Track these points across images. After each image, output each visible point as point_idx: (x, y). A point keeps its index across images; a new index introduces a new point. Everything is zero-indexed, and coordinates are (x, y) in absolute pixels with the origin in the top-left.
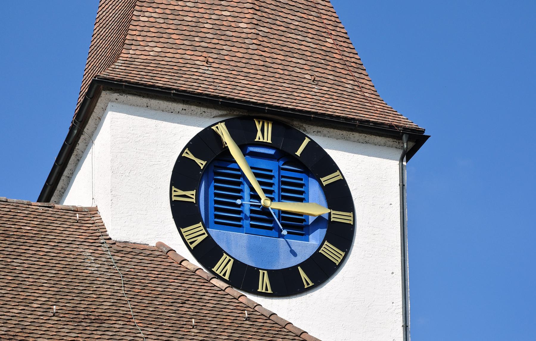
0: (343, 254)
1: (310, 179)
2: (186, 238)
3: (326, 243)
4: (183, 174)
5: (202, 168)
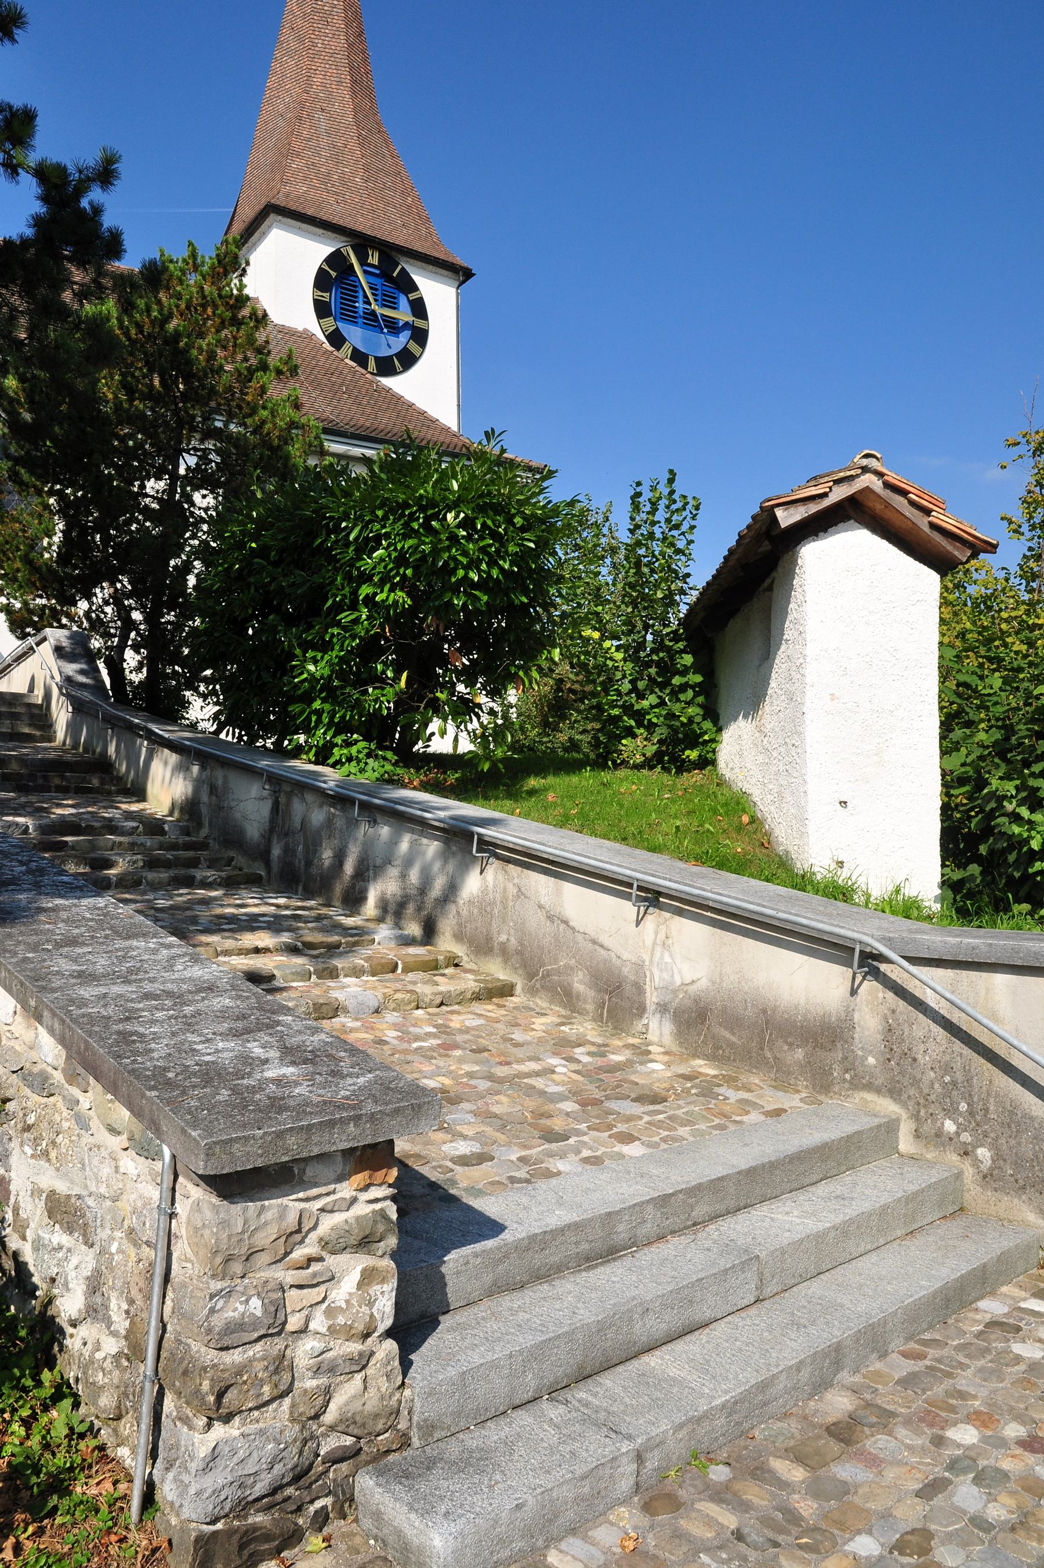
4: (322, 281)
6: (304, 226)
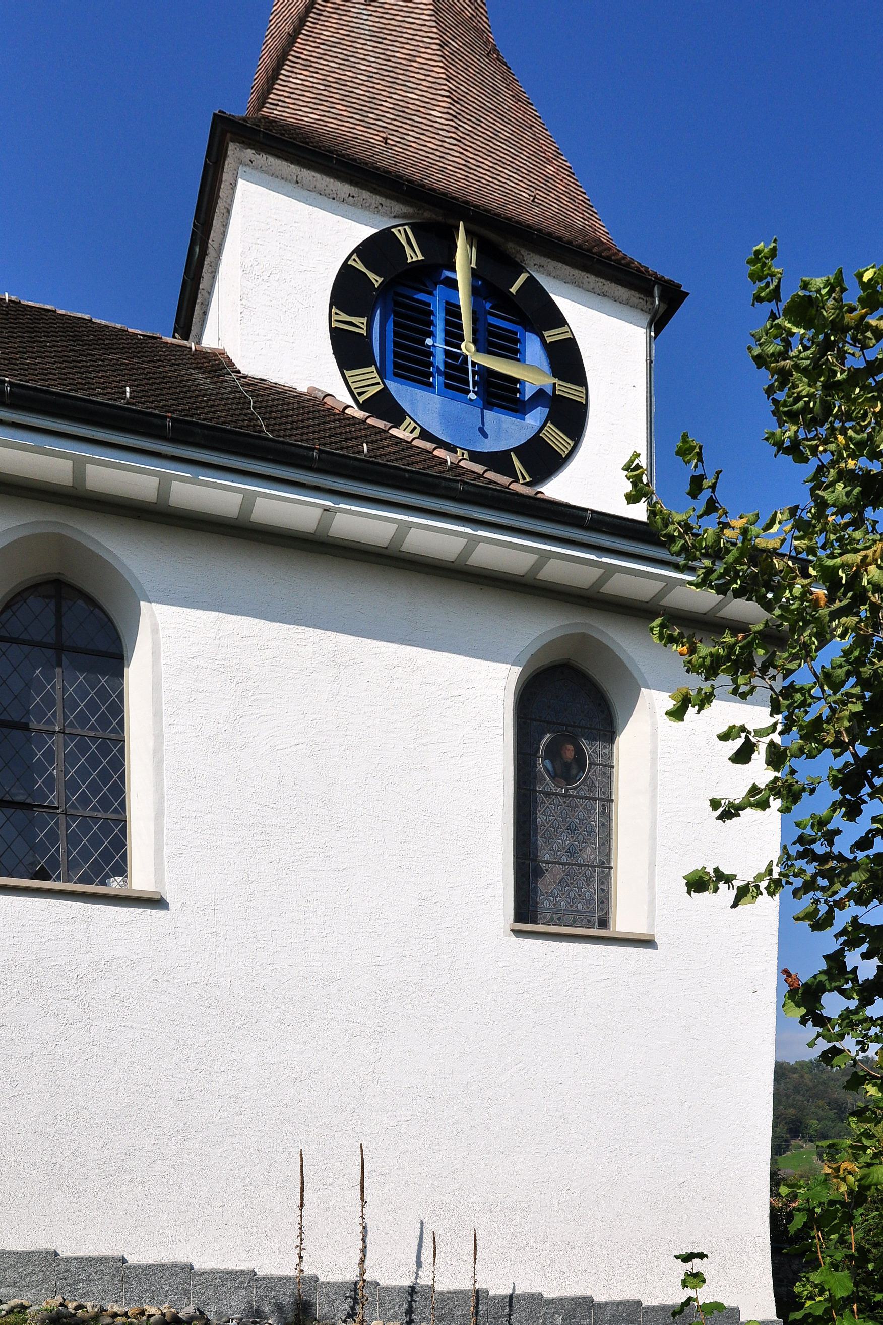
2: (353, 386)
4: (347, 291)
6: (307, 175)
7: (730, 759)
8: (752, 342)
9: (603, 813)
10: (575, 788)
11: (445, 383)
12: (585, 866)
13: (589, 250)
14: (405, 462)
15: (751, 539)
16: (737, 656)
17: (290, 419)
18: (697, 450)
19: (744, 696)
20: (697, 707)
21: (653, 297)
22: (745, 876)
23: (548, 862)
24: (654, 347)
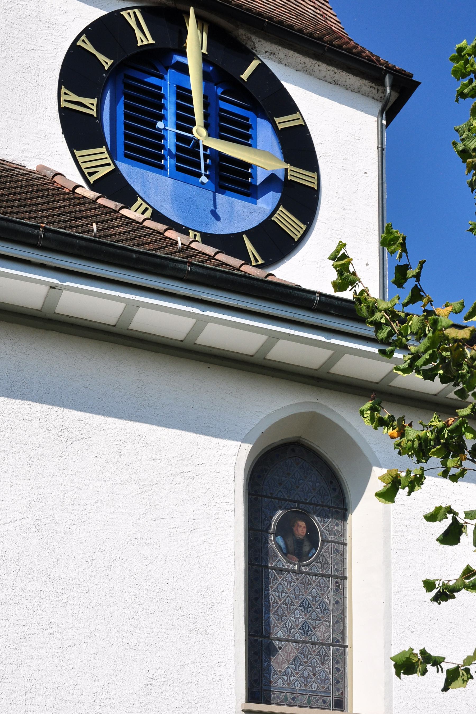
0: (304, 227)
1: (259, 120)
2: (83, 166)
3: (281, 208)
5: (106, 68)
7: (438, 540)
8: (457, 138)
9: (337, 590)
10: (307, 565)
11: (177, 166)
12: (320, 644)
13: (320, 39)
14: (135, 242)
15: (441, 330)
16: (446, 439)
17: (18, 197)
18: (401, 241)
19: (454, 478)
20: (407, 489)
21: (383, 85)
22: (454, 659)
23: (281, 640)
24: (385, 134)
